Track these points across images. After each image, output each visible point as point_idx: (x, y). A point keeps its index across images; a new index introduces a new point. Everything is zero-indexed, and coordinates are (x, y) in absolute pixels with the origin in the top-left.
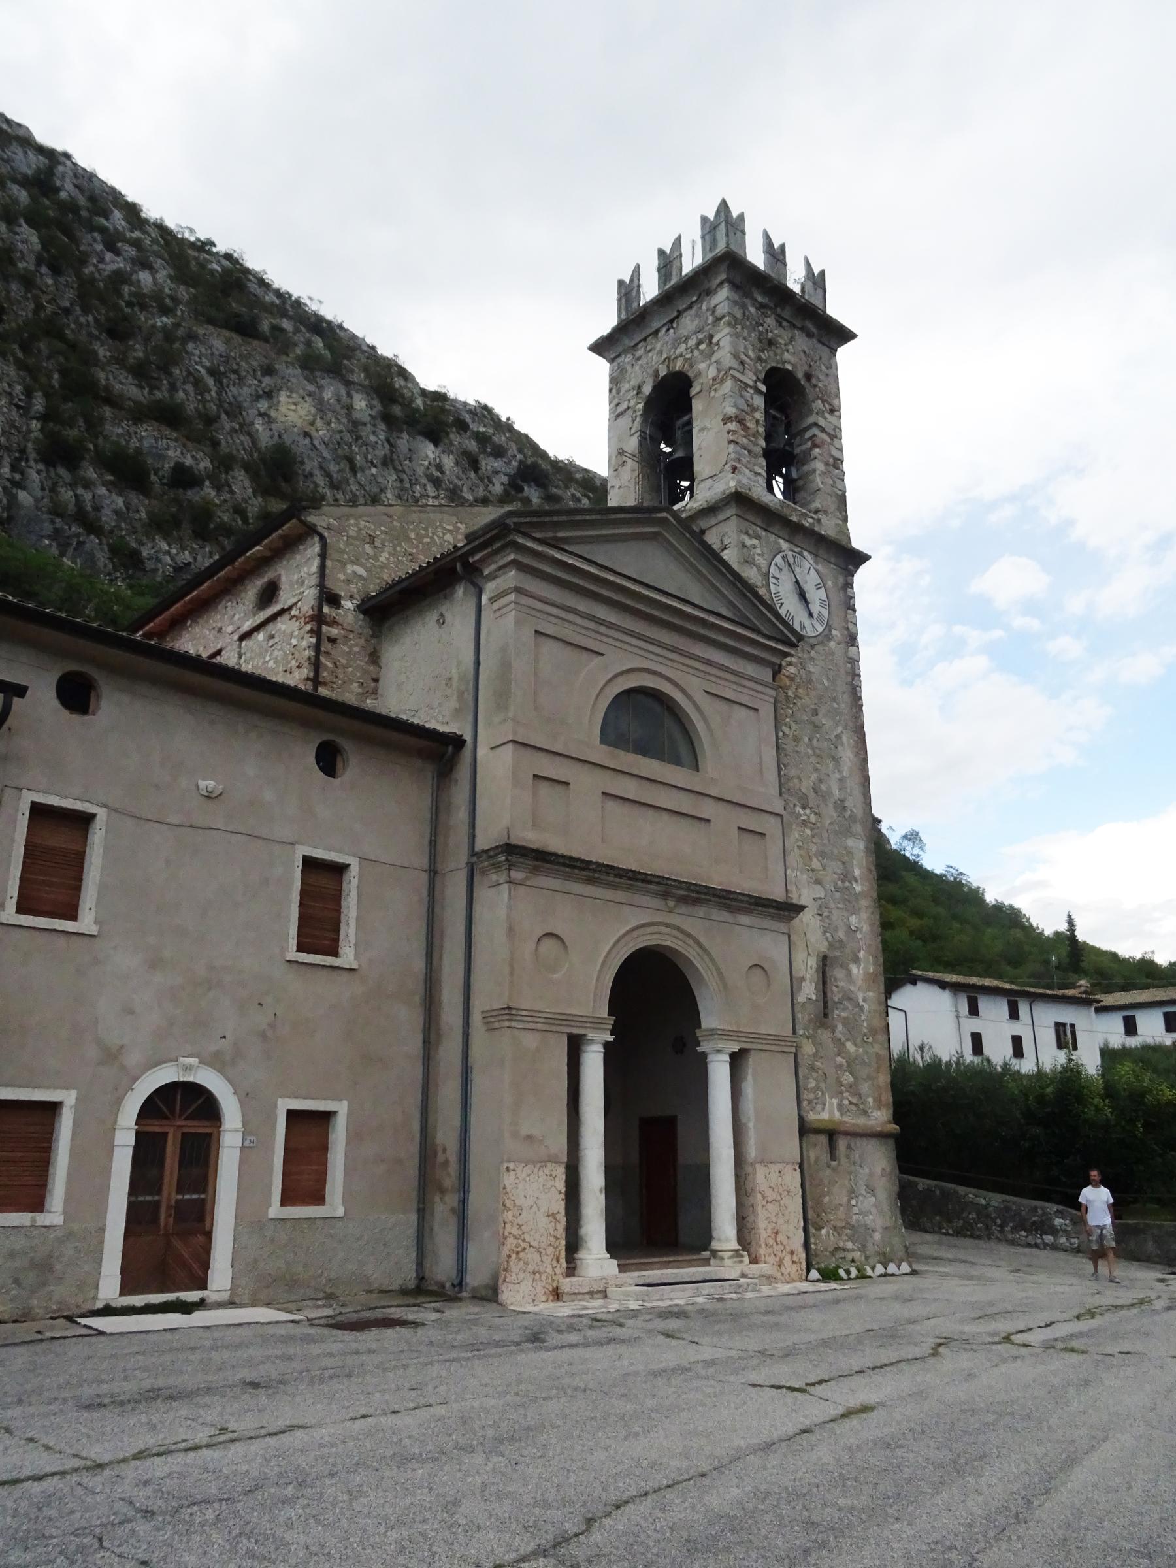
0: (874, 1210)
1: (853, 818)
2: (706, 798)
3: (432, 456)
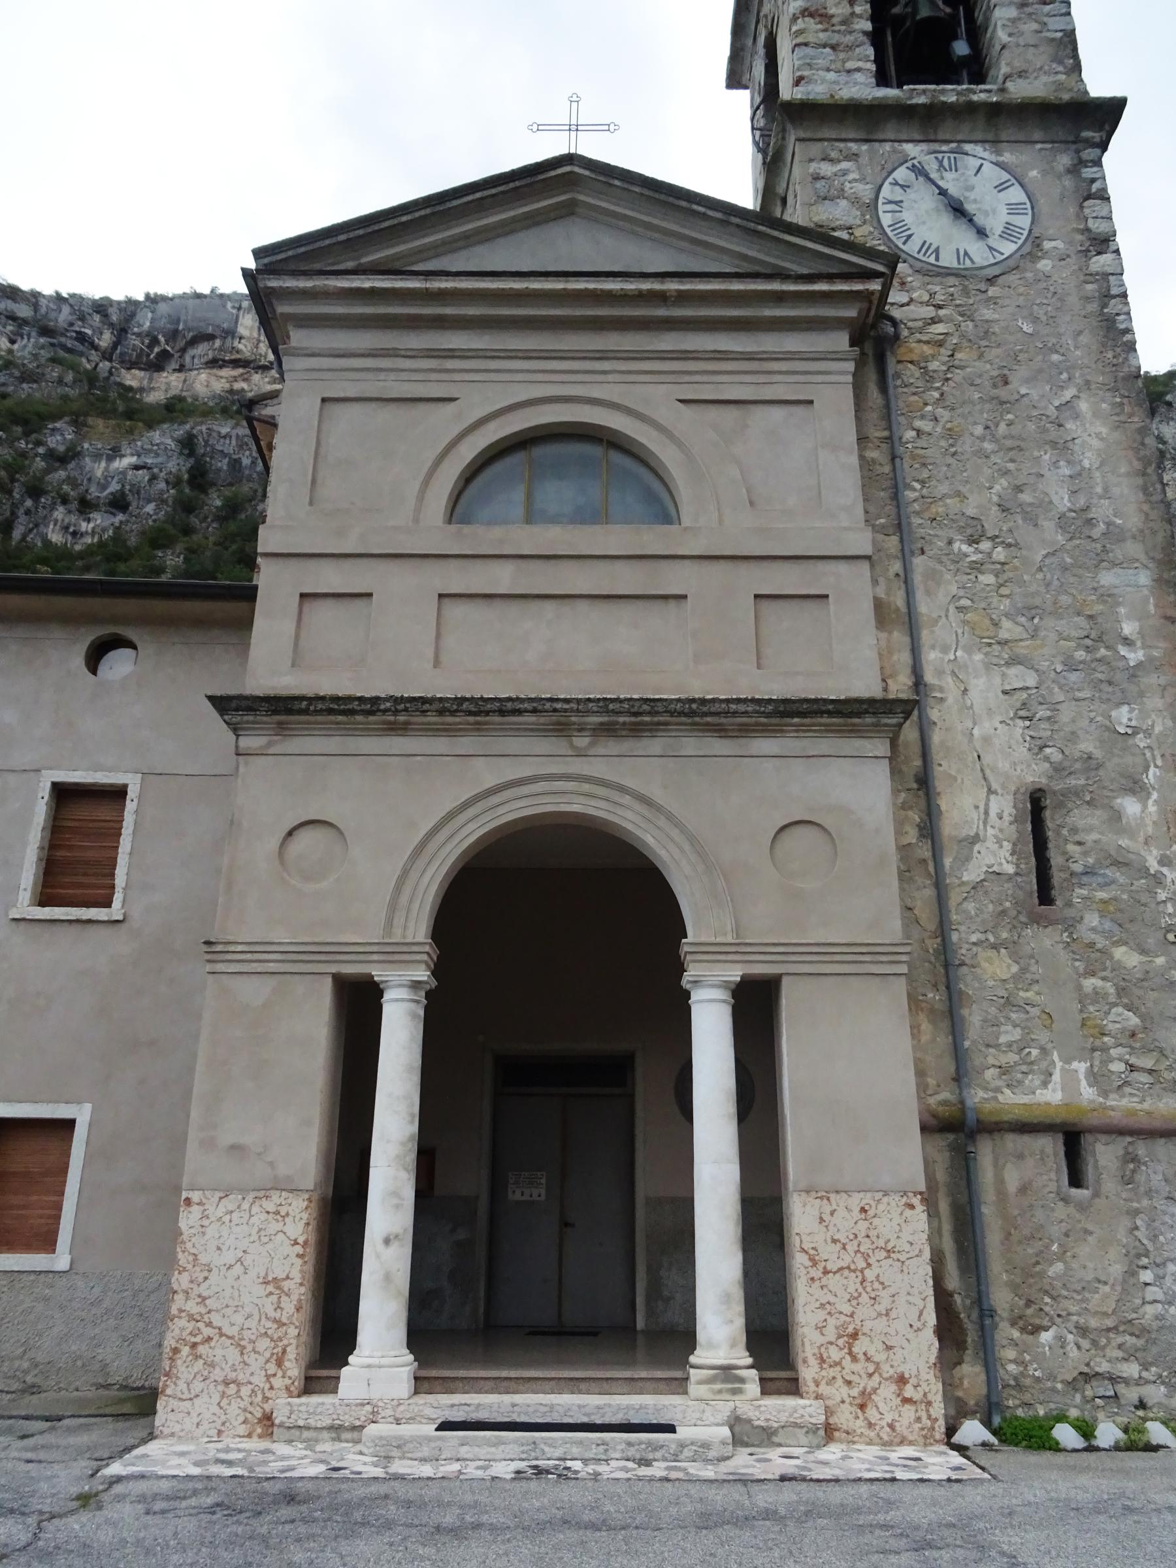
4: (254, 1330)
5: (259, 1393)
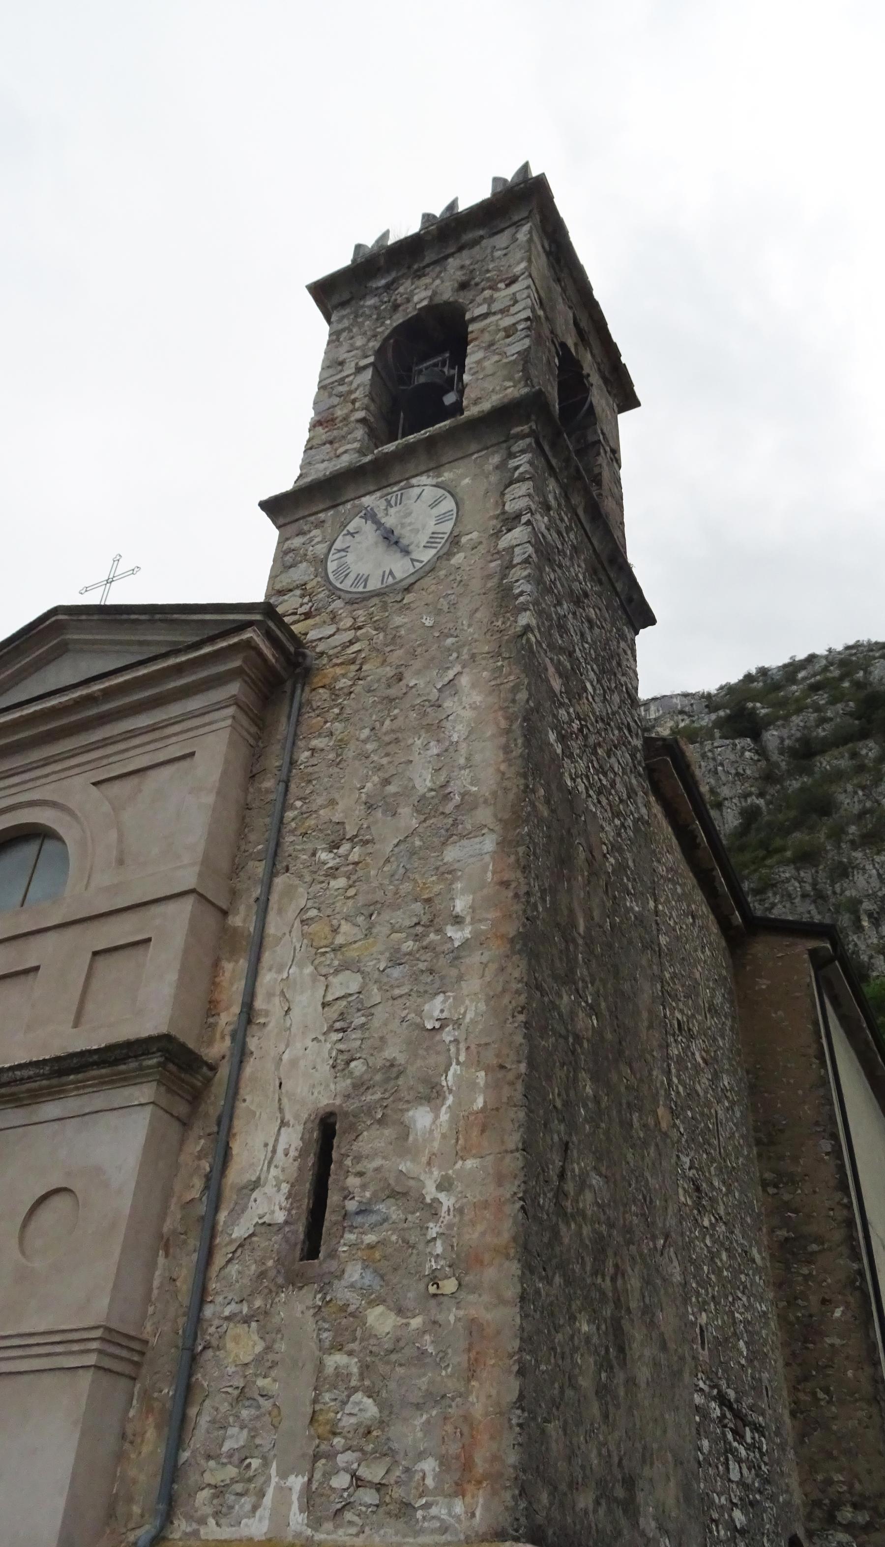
2: (32, 939)
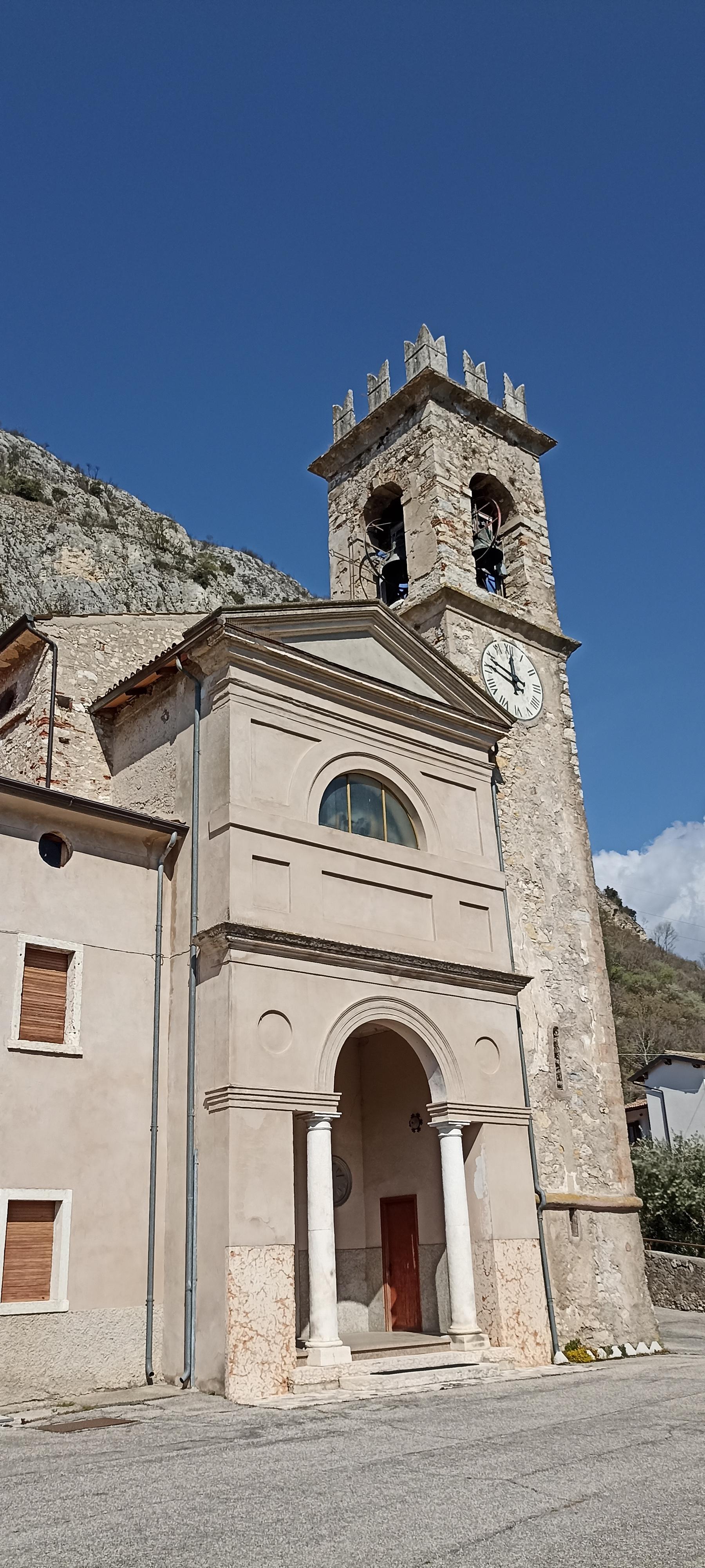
0: (620, 1288)
1: (577, 892)
3: (201, 597)
4: (273, 1330)
5: (280, 1368)
